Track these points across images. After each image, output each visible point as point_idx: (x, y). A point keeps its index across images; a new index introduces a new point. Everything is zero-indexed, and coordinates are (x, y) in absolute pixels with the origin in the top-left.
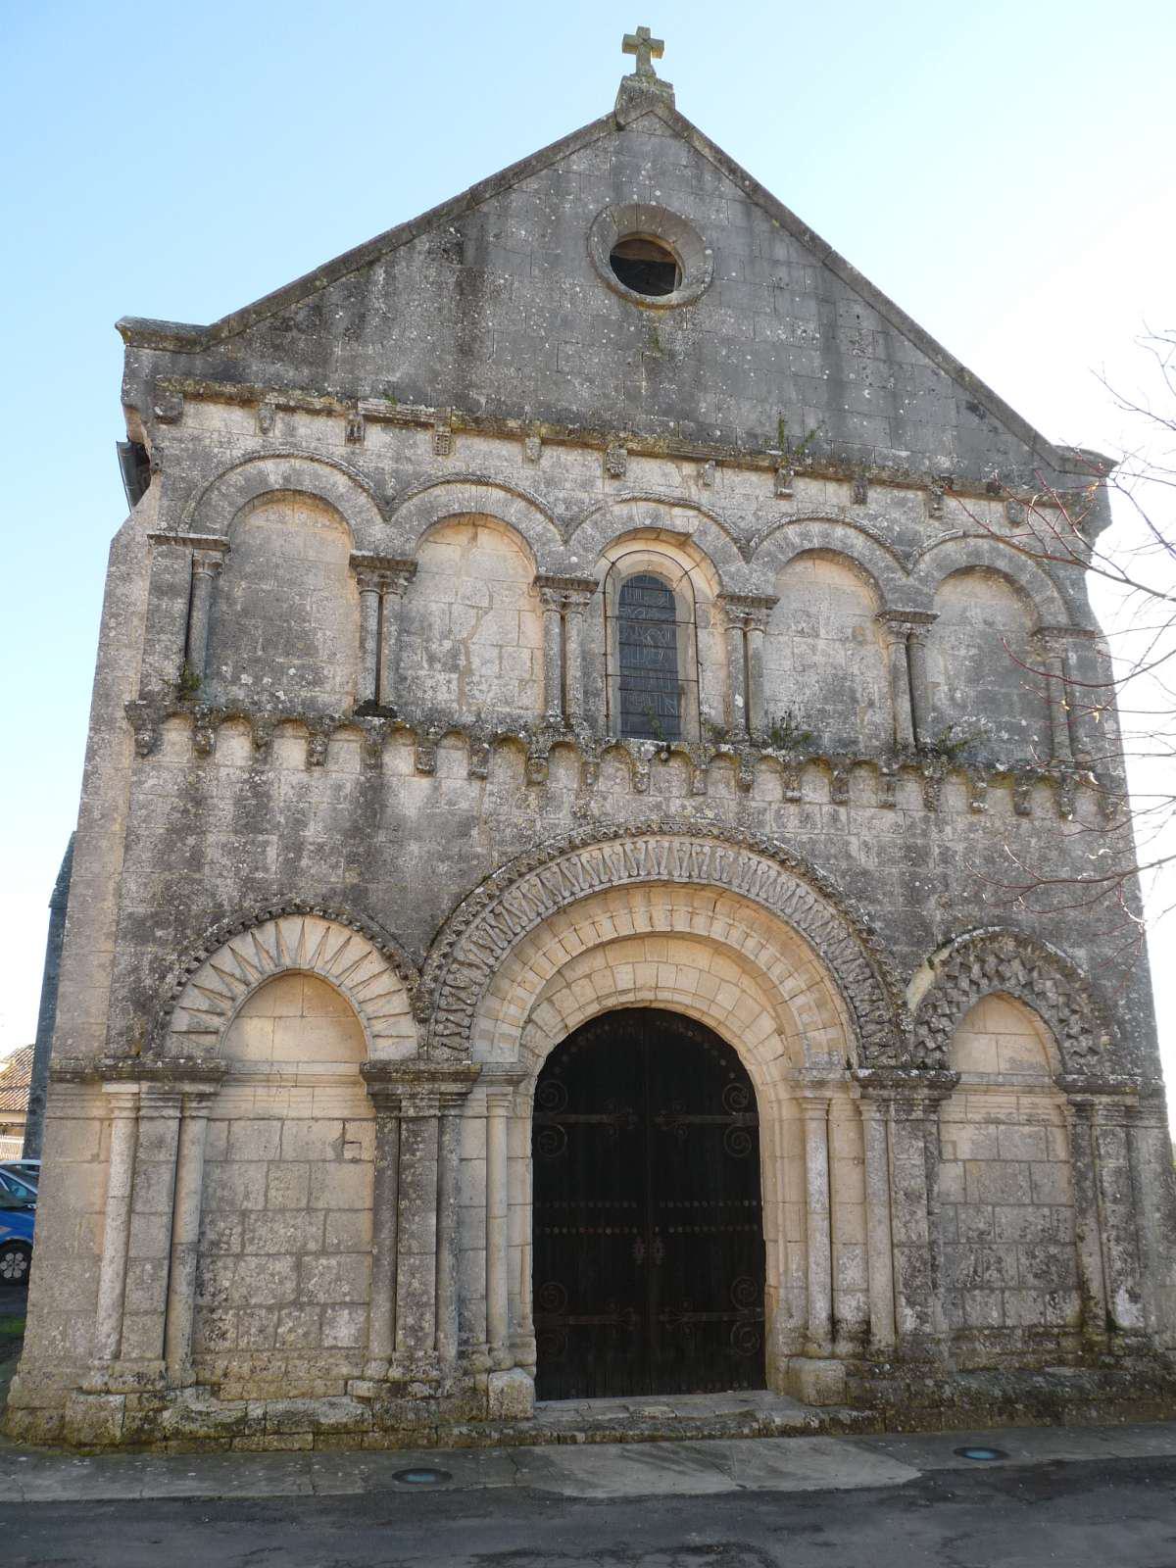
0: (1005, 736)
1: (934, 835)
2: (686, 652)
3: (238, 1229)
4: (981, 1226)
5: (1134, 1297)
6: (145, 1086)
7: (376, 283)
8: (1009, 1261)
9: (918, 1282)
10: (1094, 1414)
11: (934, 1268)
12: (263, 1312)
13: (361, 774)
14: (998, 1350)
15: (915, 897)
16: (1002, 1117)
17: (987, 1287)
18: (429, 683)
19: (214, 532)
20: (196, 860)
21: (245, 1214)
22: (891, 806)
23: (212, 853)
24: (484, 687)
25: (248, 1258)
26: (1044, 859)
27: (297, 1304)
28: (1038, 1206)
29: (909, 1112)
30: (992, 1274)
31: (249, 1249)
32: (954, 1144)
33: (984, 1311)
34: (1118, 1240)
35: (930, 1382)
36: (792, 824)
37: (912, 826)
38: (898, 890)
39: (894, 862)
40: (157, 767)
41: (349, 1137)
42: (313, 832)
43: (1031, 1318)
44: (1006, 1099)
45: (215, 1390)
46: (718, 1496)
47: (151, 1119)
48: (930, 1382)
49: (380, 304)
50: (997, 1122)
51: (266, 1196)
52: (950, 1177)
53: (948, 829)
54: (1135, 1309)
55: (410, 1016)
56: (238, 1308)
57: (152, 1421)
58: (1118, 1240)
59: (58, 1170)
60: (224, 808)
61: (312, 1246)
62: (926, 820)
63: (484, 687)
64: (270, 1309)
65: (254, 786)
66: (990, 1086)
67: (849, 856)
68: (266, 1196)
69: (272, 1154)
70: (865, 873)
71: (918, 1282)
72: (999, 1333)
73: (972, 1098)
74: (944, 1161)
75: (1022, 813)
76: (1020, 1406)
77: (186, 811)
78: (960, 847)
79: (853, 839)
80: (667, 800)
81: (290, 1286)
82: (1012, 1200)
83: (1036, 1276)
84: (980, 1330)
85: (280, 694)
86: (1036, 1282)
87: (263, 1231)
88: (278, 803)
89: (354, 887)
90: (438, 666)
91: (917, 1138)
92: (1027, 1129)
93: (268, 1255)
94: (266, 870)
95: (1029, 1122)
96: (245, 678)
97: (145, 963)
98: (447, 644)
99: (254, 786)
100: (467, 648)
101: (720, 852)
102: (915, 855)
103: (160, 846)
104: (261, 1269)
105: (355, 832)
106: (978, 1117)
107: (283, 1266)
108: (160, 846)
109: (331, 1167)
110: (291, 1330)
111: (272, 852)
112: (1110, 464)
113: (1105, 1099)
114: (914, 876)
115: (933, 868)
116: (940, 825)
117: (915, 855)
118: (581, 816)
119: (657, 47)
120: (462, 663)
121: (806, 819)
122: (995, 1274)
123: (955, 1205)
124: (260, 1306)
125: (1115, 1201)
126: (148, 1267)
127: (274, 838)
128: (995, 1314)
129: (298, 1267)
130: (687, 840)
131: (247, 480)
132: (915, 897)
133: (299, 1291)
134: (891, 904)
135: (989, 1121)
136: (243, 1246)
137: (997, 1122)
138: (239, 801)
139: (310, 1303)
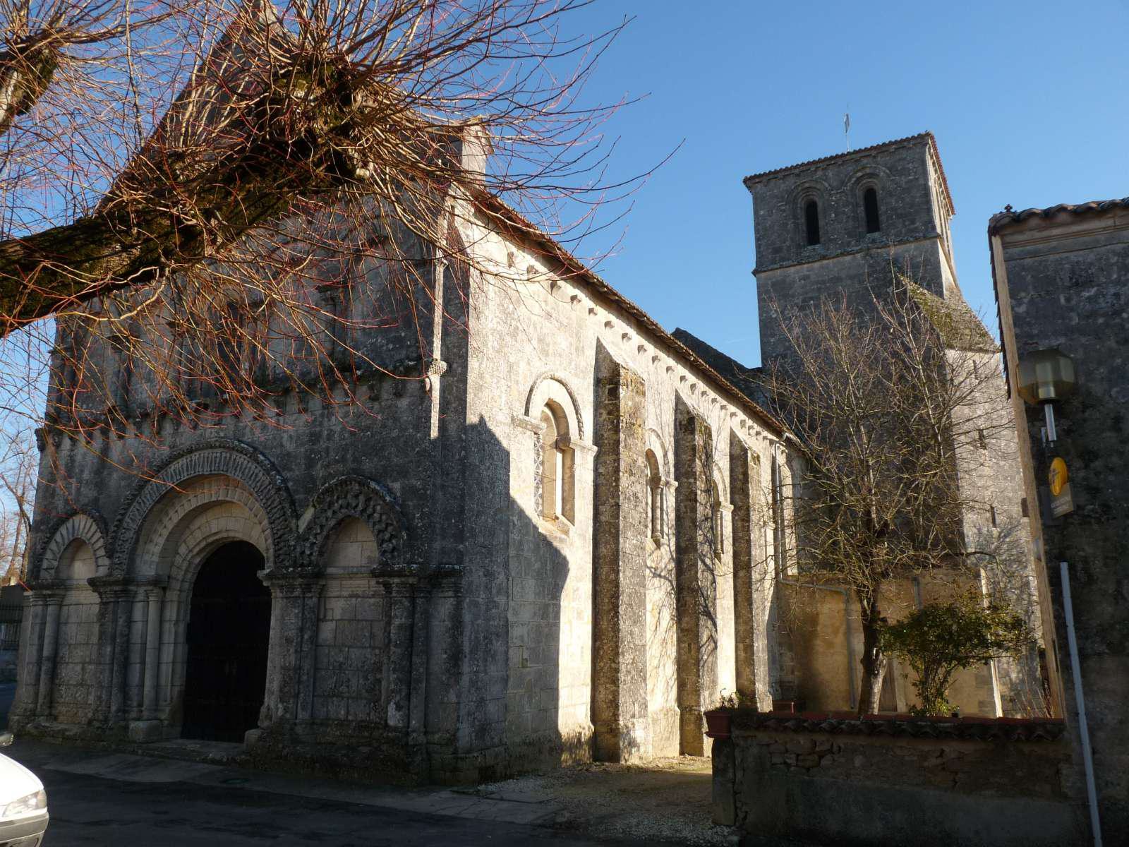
0: (391, 346)
1: (326, 424)
4: (341, 659)
5: (399, 708)
8: (354, 682)
9: (286, 690)
10: (356, 775)
11: (299, 682)
14: (338, 733)
15: (310, 463)
16: (360, 593)
17: (340, 696)
21: (70, 645)
22: (306, 410)
26: (384, 426)
27: (81, 685)
28: (374, 648)
29: (292, 592)
30: (343, 689)
32: (333, 609)
33: (338, 710)
34: (394, 670)
36: (258, 432)
37: (314, 421)
38: (303, 461)
39: (303, 444)
43: (361, 716)
44: (363, 582)
45: (56, 718)
48: (281, 746)
50: (357, 596)
52: (327, 631)
53: (334, 418)
54: (398, 715)
58: (394, 670)
62: (322, 415)
66: (352, 575)
67: (282, 445)
70: (289, 454)
71: (286, 690)
72: (342, 724)
73: (344, 582)
74: (327, 621)
75: (375, 398)
76: (317, 765)
78: (338, 429)
82: (359, 644)
83: (367, 691)
84: (334, 720)
86: (366, 695)
88: (77, 464)
91: (295, 607)
92: (372, 601)
95: (373, 596)
101: (224, 455)
102: (314, 437)
106: (345, 594)
107: (78, 668)
113: (396, 580)
114: (312, 451)
115: (323, 444)
116: (330, 415)
118: (172, 447)
121: (264, 427)
122: (346, 689)
123: (329, 646)
125: (396, 646)
128: (342, 712)
129: (83, 669)
130: (210, 451)
132: (310, 463)
133: (83, 679)
134: (297, 471)
135: (351, 596)
137: (357, 596)
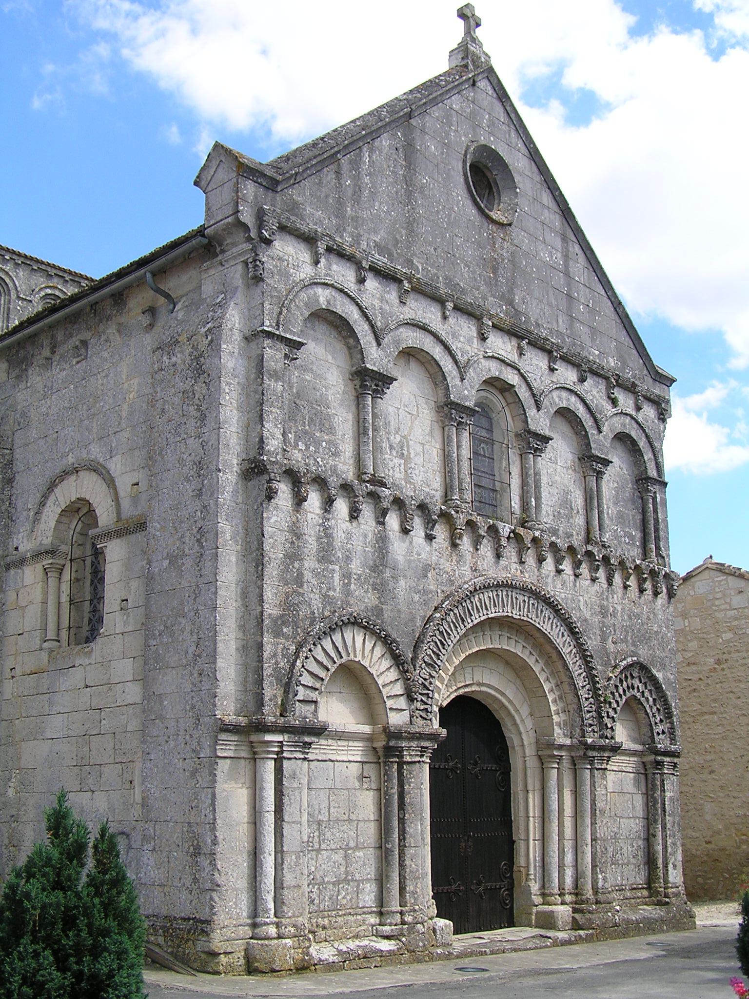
2: (501, 463)
3: (317, 834)
6: (286, 737)
7: (364, 162)
12: (331, 886)
13: (376, 528)
18: (391, 464)
19: (294, 334)
20: (299, 580)
23: (308, 576)
24: (417, 472)
25: (323, 852)
27: (346, 881)
31: (323, 846)
35: (610, 914)
38: (598, 632)
40: (276, 508)
41: (365, 774)
42: (355, 566)
46: (645, 960)
47: (290, 759)
49: (367, 179)
51: (329, 811)
55: (405, 696)
56: (319, 884)
57: (308, 954)
59: (225, 793)
60: (311, 544)
61: (352, 844)
63: (417, 472)
64: (334, 884)
65: (326, 529)
68: (329, 811)
69: (330, 784)
77: (293, 543)
79: (581, 598)
80: (510, 563)
81: (343, 869)
85: (319, 460)
87: (328, 835)
88: (337, 544)
89: (377, 606)
90: (394, 453)
93: (332, 850)
94: (335, 590)
96: (301, 446)
97: (279, 650)
98: (398, 438)
99: (326, 529)
100: (407, 442)
103: (281, 567)
104: (329, 858)
105: (374, 569)
107: (338, 857)
108: (281, 567)
109: (358, 793)
110: (344, 898)
111: (337, 577)
112: (673, 381)
113: (668, 759)
117: (603, 612)
119: (560, 68)
120: (405, 453)
124: (329, 882)
126: (294, 857)
127: (337, 568)
129: (346, 856)
131: (309, 298)
133: (347, 873)
136: (320, 845)
138: (319, 538)
139: (352, 880)
